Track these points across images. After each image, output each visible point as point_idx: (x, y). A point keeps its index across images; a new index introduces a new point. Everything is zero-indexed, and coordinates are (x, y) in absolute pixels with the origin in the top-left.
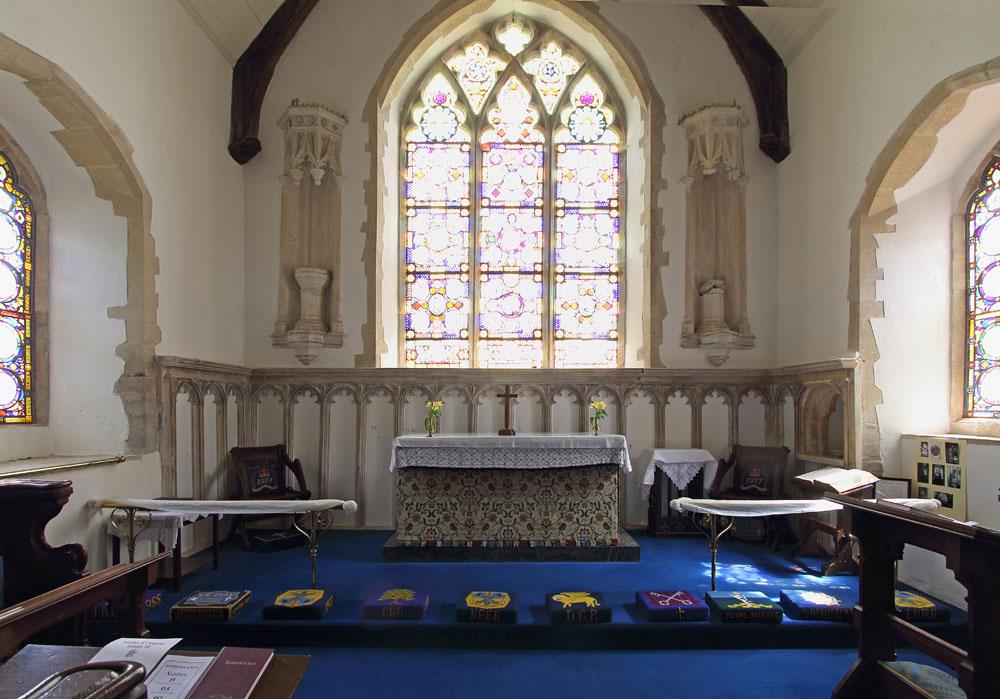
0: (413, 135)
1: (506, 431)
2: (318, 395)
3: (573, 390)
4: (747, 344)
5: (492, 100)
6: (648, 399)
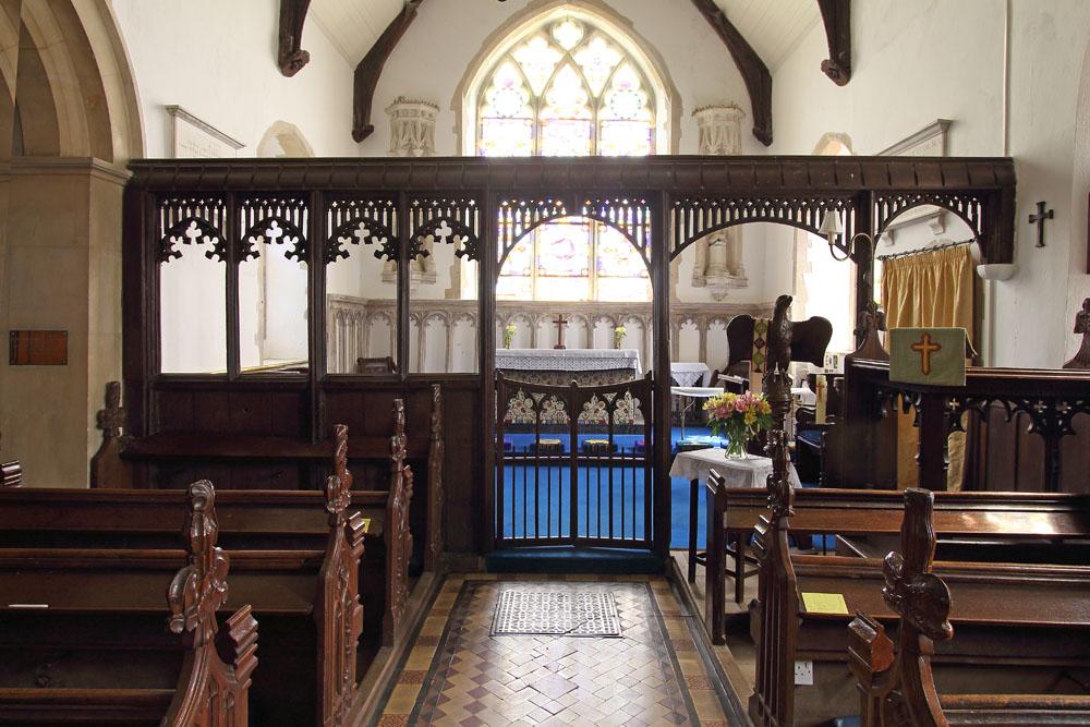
0: (485, 112)
1: (559, 346)
3: (610, 318)
4: (742, 285)
5: (550, 85)
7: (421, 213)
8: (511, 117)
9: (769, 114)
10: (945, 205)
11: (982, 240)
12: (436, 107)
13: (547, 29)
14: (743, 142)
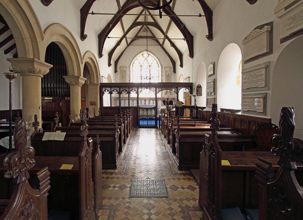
3: (153, 100)
13: (143, 55)
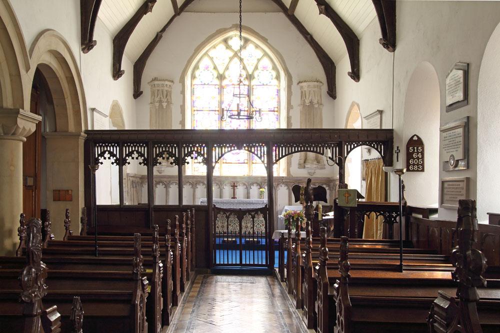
1: (234, 198)
2: (165, 185)
3: (258, 184)
5: (227, 68)
6: (286, 187)
7: (186, 149)
8: (208, 84)
9: (335, 84)
10: (370, 146)
11: (383, 158)
12: (172, 81)
13: (225, 41)
14: (323, 96)
